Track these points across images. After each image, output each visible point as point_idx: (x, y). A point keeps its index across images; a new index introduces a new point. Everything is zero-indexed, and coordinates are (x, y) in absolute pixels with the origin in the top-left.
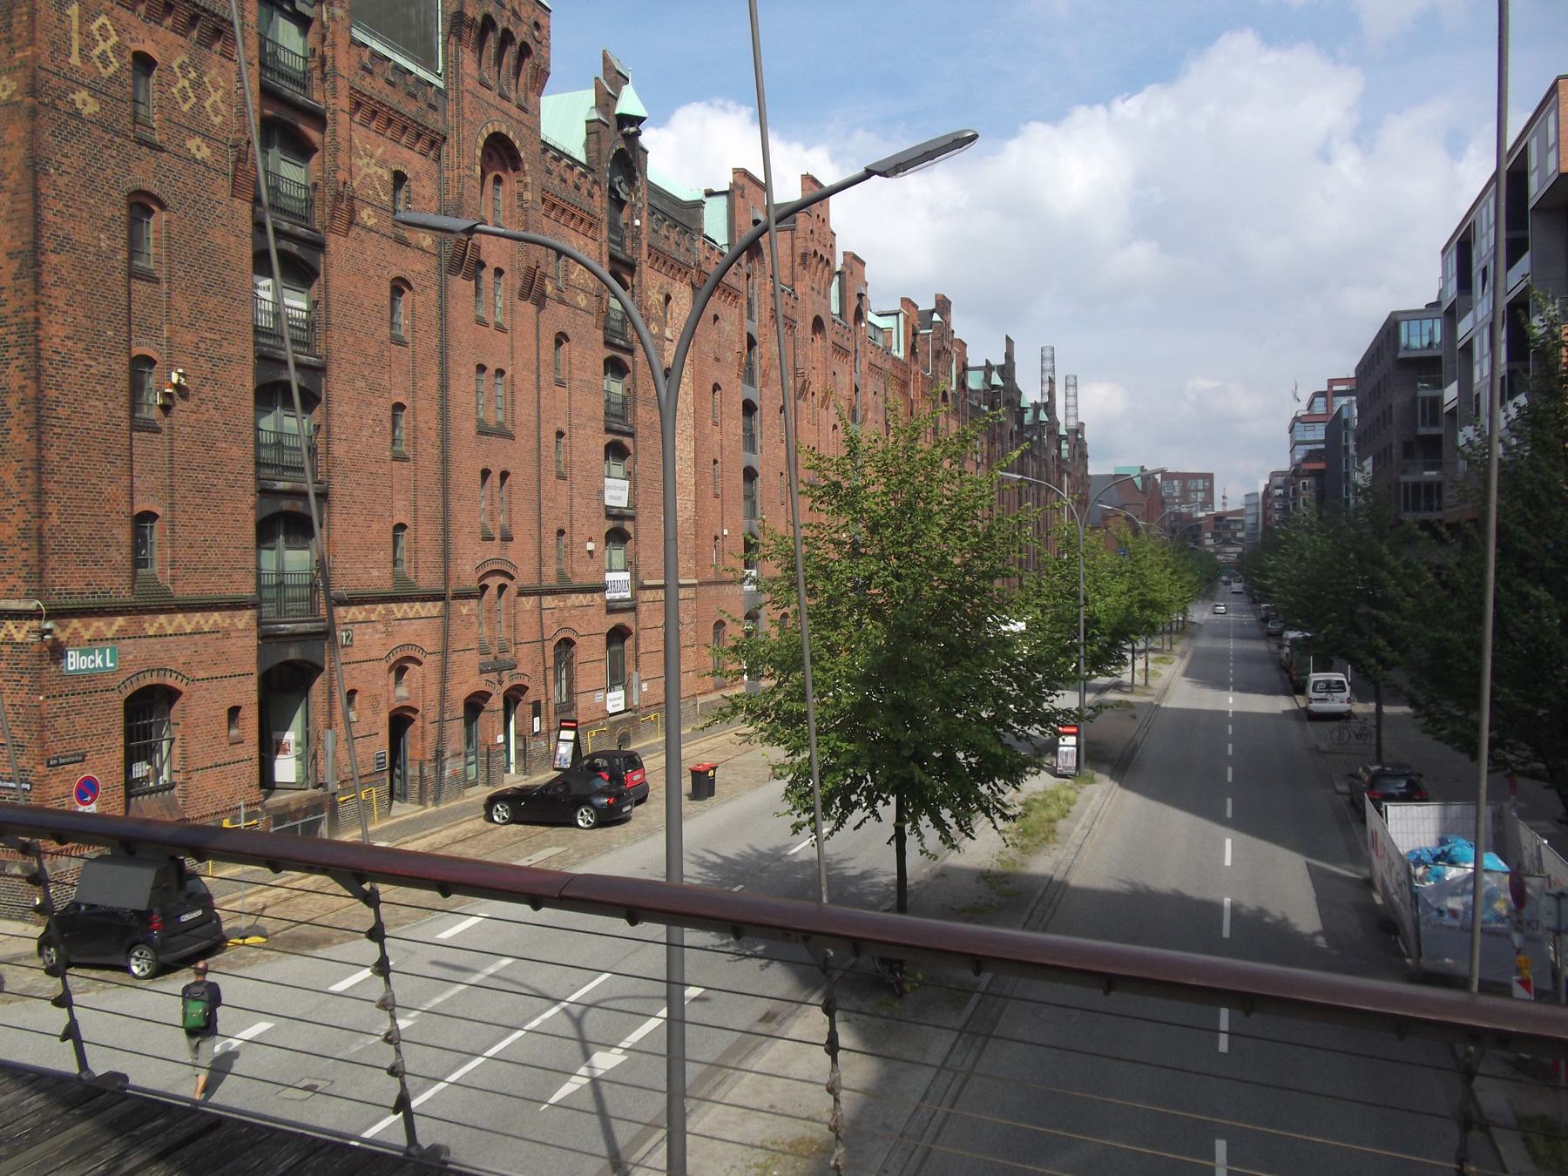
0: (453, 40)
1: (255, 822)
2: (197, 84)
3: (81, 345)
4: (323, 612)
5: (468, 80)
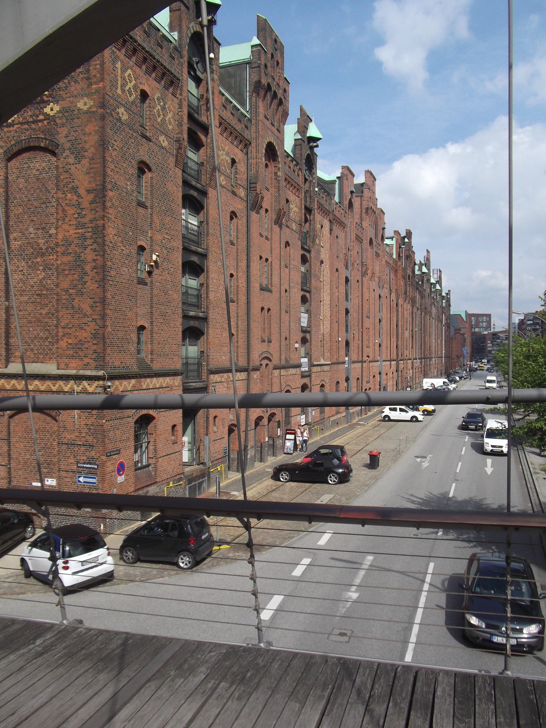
0: (254, 95)
1: (181, 483)
2: (163, 108)
3: (120, 239)
4: (204, 377)
5: (261, 115)
